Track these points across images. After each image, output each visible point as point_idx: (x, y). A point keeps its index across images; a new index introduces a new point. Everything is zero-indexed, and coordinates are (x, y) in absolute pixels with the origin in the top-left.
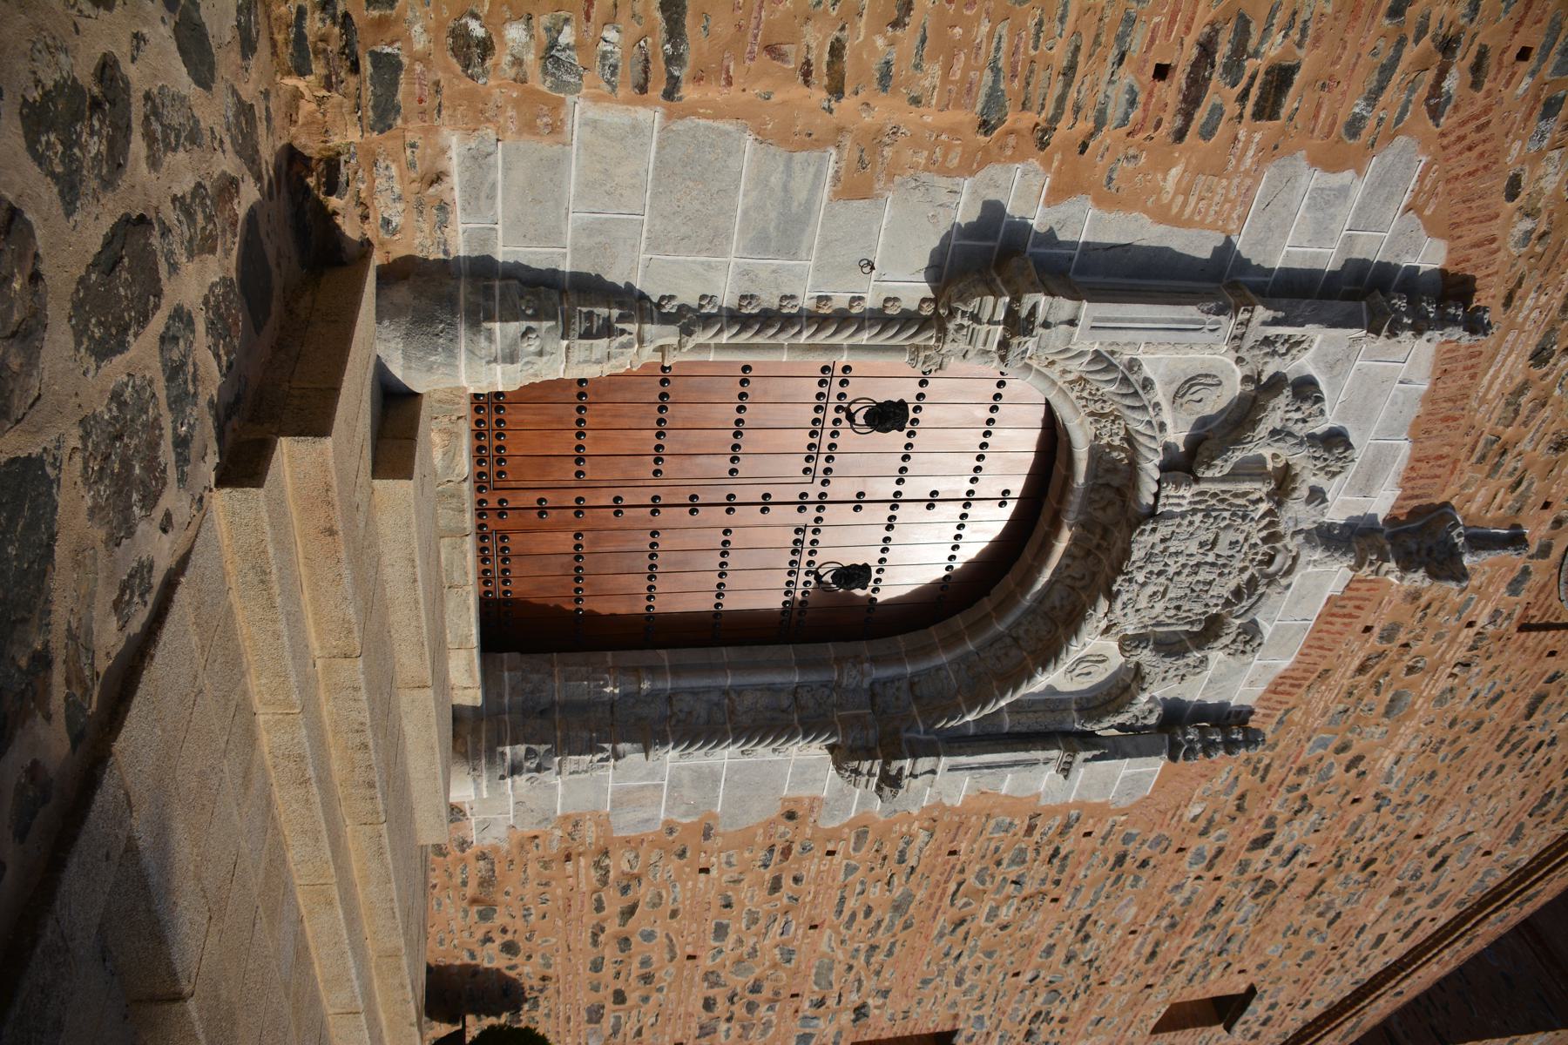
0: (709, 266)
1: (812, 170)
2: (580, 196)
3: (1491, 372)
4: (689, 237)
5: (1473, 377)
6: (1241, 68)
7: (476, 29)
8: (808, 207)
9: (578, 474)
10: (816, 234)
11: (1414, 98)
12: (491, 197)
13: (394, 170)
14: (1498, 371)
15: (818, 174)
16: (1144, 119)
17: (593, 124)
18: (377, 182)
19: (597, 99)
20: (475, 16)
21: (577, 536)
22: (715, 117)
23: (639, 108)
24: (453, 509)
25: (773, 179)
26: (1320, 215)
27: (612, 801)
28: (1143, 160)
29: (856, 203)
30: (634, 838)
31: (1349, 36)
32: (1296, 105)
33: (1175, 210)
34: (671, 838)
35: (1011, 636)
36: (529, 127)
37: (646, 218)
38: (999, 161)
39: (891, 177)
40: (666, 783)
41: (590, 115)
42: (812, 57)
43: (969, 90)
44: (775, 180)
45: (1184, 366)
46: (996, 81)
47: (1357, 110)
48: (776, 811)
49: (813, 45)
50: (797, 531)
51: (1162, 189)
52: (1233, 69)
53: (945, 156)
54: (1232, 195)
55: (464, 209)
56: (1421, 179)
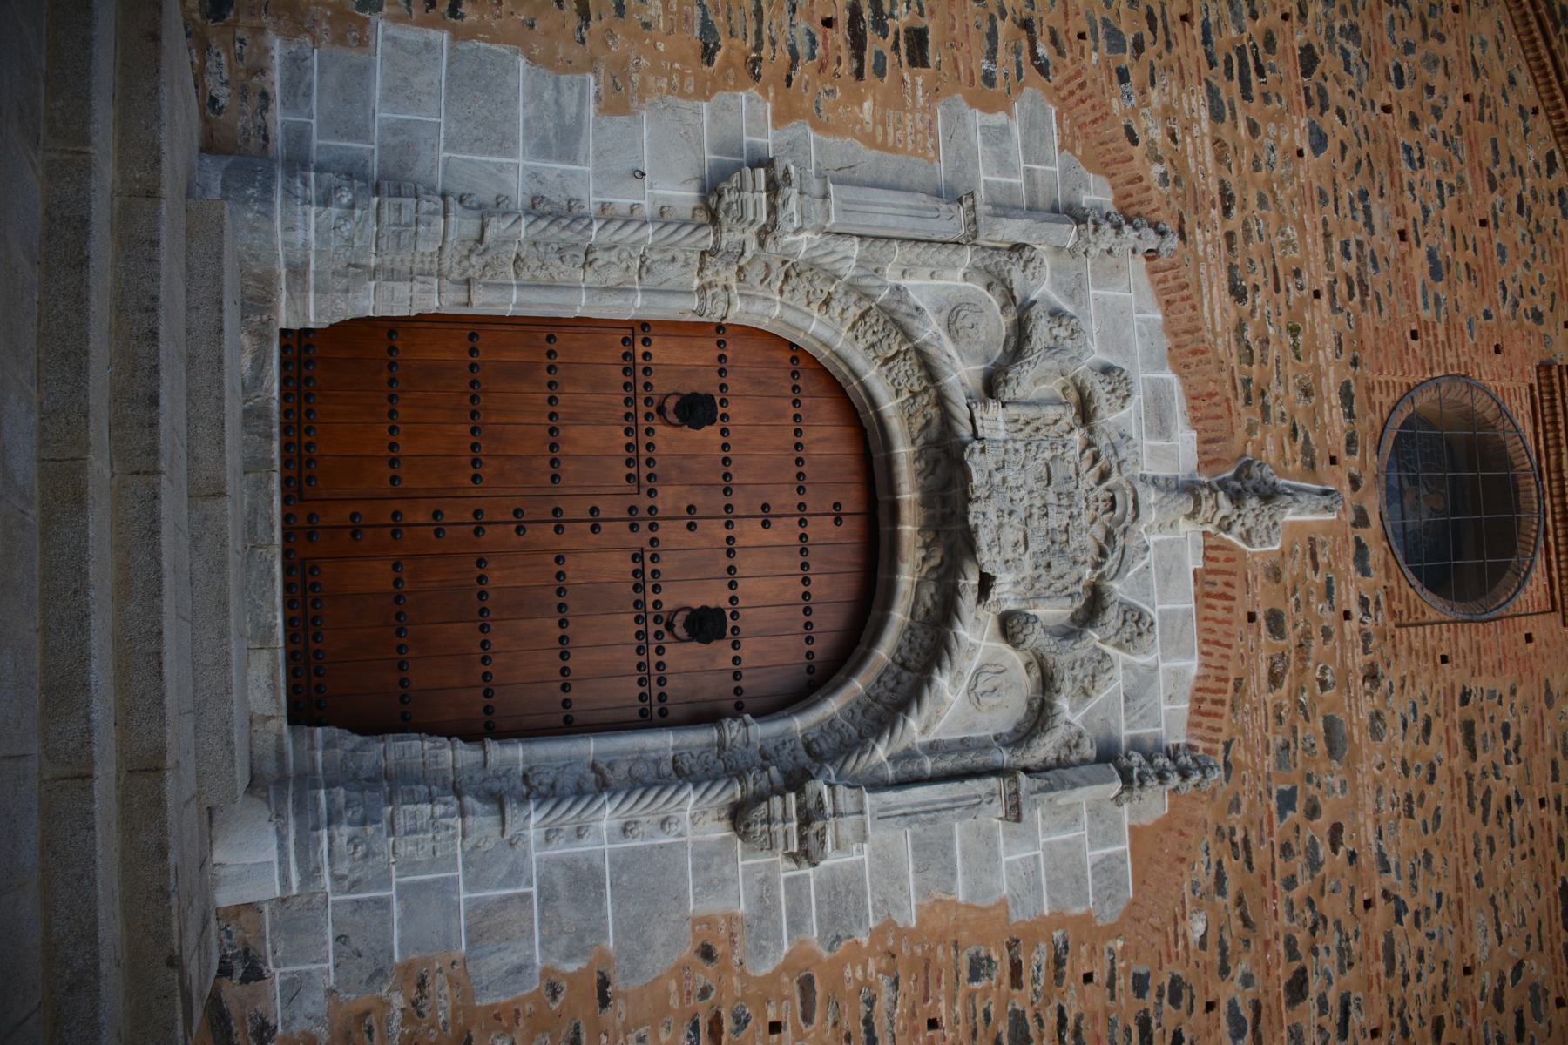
0: (501, 167)
1: (577, 89)
2: (384, 99)
3: (1206, 301)
4: (481, 140)
8: (579, 118)
9: (393, 479)
10: (589, 143)
11: (1021, 58)
12: (308, 95)
13: (224, 59)
14: (1211, 301)
15: (582, 94)
16: (827, 55)
17: (394, 40)
18: (209, 64)
19: (396, 19)
21: (395, 567)
22: (492, 41)
24: (260, 435)
25: (545, 95)
27: (468, 931)
28: (839, 94)
29: (618, 119)
30: (506, 1006)
31: (954, 11)
33: (880, 139)
34: (555, 1006)
36: (340, 40)
37: (442, 121)
38: (725, 90)
39: (642, 99)
40: (534, 890)
43: (687, 20)
44: (548, 95)
45: (944, 294)
46: (705, 14)
47: (985, 67)
48: (687, 951)
50: (634, 558)
53: (682, 82)
54: (920, 126)
55: (283, 103)
56: (1060, 125)
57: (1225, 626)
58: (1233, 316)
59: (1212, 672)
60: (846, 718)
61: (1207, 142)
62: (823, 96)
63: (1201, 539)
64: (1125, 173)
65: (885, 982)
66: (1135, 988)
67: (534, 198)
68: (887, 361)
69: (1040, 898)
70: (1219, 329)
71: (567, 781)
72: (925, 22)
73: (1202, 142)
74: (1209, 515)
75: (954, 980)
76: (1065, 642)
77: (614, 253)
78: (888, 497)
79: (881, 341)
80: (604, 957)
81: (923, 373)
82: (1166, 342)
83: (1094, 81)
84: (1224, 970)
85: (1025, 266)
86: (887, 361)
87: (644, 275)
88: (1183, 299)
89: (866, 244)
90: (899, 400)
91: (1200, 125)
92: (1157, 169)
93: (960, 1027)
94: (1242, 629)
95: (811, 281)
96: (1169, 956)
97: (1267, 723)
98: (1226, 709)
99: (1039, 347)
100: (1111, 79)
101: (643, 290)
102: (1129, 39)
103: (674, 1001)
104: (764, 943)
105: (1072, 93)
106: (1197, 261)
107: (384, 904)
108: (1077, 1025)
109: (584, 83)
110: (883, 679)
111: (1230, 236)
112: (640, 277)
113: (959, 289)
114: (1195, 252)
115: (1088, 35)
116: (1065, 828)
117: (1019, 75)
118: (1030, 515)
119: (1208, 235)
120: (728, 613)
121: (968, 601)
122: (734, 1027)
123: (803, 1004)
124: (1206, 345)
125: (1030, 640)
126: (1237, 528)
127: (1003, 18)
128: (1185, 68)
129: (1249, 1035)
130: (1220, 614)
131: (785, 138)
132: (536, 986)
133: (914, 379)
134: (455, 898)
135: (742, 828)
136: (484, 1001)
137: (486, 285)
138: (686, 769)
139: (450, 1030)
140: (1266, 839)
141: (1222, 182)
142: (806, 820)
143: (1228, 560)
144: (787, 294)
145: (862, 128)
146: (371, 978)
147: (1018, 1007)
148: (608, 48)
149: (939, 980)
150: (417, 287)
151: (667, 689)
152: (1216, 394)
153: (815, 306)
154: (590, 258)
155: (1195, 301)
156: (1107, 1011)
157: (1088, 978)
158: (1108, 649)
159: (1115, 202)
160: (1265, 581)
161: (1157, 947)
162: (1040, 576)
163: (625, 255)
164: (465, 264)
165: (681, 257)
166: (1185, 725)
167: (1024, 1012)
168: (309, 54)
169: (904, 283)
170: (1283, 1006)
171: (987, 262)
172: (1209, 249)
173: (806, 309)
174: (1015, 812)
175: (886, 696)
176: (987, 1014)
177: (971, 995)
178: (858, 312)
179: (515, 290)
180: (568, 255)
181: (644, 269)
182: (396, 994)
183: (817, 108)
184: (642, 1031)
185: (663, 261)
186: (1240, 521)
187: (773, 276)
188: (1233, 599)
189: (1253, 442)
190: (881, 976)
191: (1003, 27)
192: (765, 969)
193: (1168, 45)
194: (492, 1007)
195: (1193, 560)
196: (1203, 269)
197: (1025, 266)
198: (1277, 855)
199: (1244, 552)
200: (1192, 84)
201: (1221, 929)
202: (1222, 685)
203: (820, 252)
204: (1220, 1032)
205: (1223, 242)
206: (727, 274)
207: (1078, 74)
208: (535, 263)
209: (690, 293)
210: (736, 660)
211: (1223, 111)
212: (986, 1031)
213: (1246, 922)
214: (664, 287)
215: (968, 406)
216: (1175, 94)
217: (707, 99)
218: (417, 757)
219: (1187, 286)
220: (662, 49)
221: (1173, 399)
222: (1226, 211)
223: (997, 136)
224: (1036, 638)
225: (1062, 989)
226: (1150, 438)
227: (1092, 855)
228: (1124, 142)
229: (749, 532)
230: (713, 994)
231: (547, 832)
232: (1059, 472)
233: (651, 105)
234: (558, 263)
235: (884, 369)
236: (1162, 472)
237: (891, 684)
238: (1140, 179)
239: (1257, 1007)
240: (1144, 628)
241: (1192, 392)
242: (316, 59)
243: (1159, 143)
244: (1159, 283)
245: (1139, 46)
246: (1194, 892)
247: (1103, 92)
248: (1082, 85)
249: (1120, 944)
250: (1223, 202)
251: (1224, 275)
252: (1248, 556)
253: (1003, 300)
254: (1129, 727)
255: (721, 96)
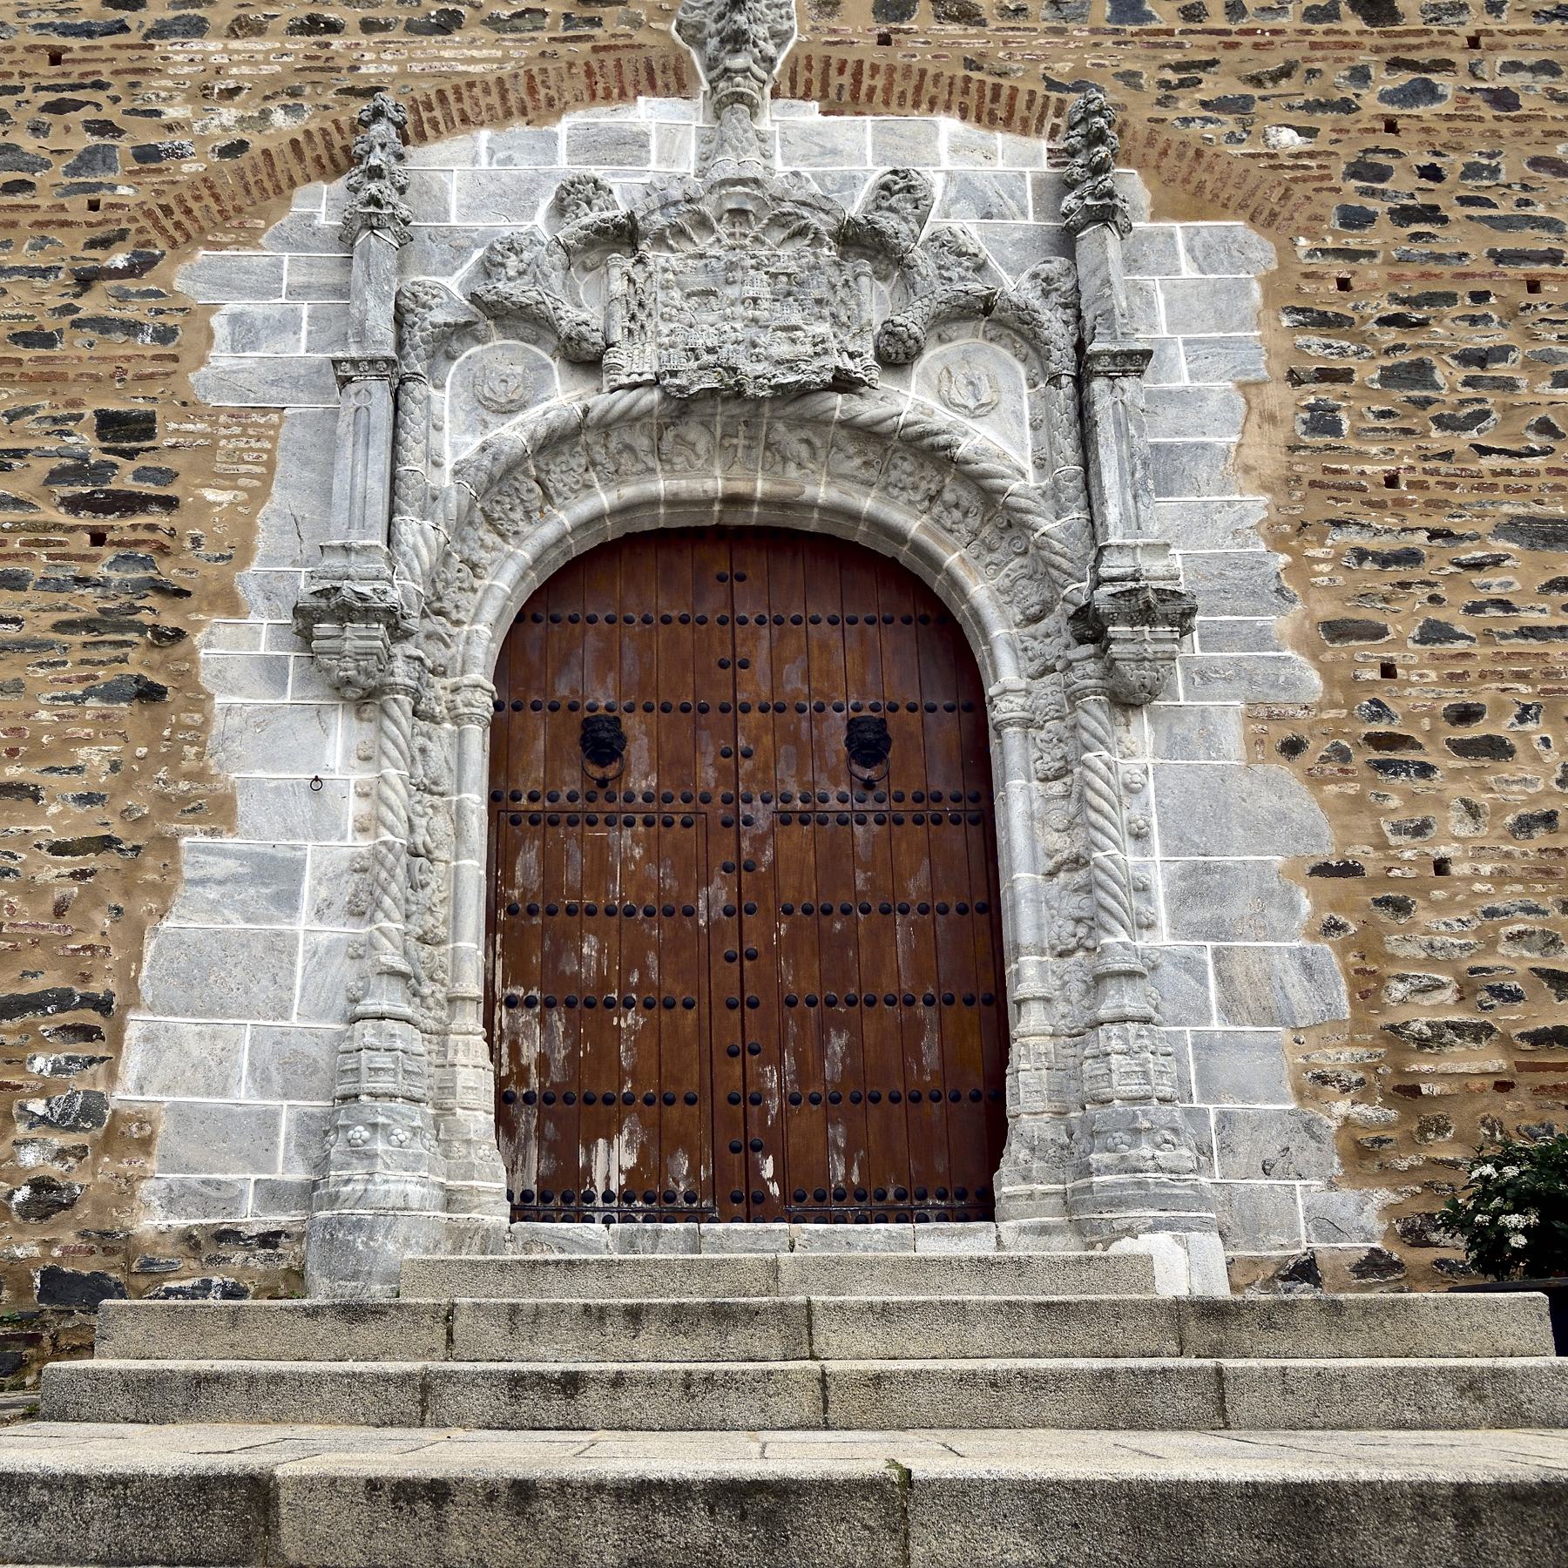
1: (202, 858)
3: (461, 68)
5: (471, 85)
6: (98, 466)
7: (23, 1193)
11: (133, 290)
12: (219, 1185)
15: (208, 851)
19: (112, 1076)
20: (10, 1195)
23: (127, 1035)
25: (211, 896)
26: (263, 333)
28: (198, 532)
29: (241, 807)
30: (1353, 985)
32: (141, 400)
33: (256, 483)
34: (1353, 928)
35: (930, 509)
36: (145, 1144)
38: (197, 675)
41: (130, 1085)
42: (66, 871)
44: (212, 893)
45: (461, 415)
48: (1285, 771)
49: (56, 872)
51: (231, 503)
52: (102, 471)
54: (237, 430)
57: (897, 76)
58: (481, 32)
59: (957, 98)
60: (996, 572)
61: (235, 44)
62: (202, 551)
63: (781, 102)
64: (286, 163)
65: (1337, 537)
66: (1361, 226)
67: (352, 914)
68: (547, 497)
69: (1239, 340)
70: (499, 54)
71: (1075, 904)
72: (88, 413)
73: (238, 52)
74: (755, 84)
75: (1337, 452)
76: (918, 287)
77: (417, 821)
78: (717, 508)
79: (522, 501)
80: (1286, 873)
81: (565, 449)
82: (518, 127)
83: (159, 193)
84: (1346, 106)
85: (424, 306)
86: (547, 497)
87: (440, 789)
88: (459, 99)
89: (404, 506)
90: (597, 485)
91: (212, 53)
92: (279, 118)
93: (1398, 449)
94: (899, 55)
95: (447, 583)
96: (1322, 178)
97: (1025, 29)
98: (1006, 83)
99: (534, 294)
100: (154, 171)
101: (459, 791)
102: (94, 140)
103: (1352, 789)
104: (1282, 679)
105: (178, 225)
106: (404, 74)
107: (1225, 1118)
108: (1403, 302)
109: (193, 849)
110: (948, 525)
111: (368, 26)
112: (442, 795)
113: (455, 396)
114: (394, 77)
115: (93, 196)
116: (1150, 304)
117: (158, 294)
118: (755, 320)
119: (368, 56)
120: (853, 714)
121: (866, 409)
122: (1386, 720)
123: (1360, 638)
124: (521, 72)
125: (915, 329)
126: (770, 49)
127: (77, 310)
128: (131, 66)
129: (1434, 78)
130: (880, 82)
131: (261, 603)
132: (1327, 947)
133: (574, 463)
134: (1218, 1036)
135: (1144, 695)
136: (1346, 1011)
137: (455, 979)
138: (1057, 765)
139: (1380, 1050)
140: (1178, 38)
141: (292, 30)
142: (1146, 615)
143: (809, 67)
144: (462, 616)
145: (243, 504)
146: (1313, 1136)
147: (1376, 376)
148: (144, 818)
149: (1336, 471)
150: (461, 1058)
151: (947, 792)
152: (587, 64)
153: (477, 583)
154: (423, 851)
155: (462, 82)
156: (1388, 262)
157: (1344, 284)
158: (925, 234)
159: (328, 180)
160: (836, 19)
161: (1311, 193)
162: (832, 315)
163: (419, 808)
164: (431, 1001)
165: (420, 741)
166: (1024, 139)
167: (1383, 368)
168: (163, 1184)
169: (449, 465)
170: (1397, 28)
171: (421, 352)
172: (389, 57)
173: (480, 594)
174: (1136, 361)
175: (973, 522)
176: (1383, 415)
177: (1357, 434)
178: (486, 526)
179: (459, 944)
180: (419, 877)
181: (434, 788)
182: (1334, 1110)
183: (217, 559)
184: (1386, 828)
185: (425, 764)
186: (761, 43)
187: (441, 630)
188: (860, 63)
189: (650, 19)
190: (1329, 542)
191: (89, 306)
192: (1315, 679)
193: (100, 86)
194: (1351, 997)
195: (808, 114)
196: (416, 68)
197: (424, 306)
198: (1198, 26)
199: (799, 43)
200: (153, 58)
201: (1290, 108)
202: (973, 87)
203: (416, 564)
204: (1426, 116)
205: (378, 37)
206: (438, 686)
207: (149, 214)
208: (430, 920)
209: (461, 734)
210: (912, 708)
211: (190, 18)
212: (1403, 417)
213: (1286, 72)
214: (453, 765)
215: (613, 391)
216: (170, 84)
217: (211, 697)
218: (1040, 1078)
219: (441, 93)
220: (145, 750)
221: (595, 124)
222: (334, 28)
223: (246, 333)
224: (912, 320)
225: (1357, 319)
226: (648, 161)
227: (1188, 270)
228: (244, 160)
229: (756, 685)
230: (1344, 743)
231: (1140, 926)
232: (700, 282)
233: (221, 767)
234: (428, 890)
235: (558, 501)
236: (692, 149)
237: (957, 514)
238: (294, 143)
239: (1395, 65)
240: (902, 184)
241: (586, 97)
242: (171, 1176)
243: (240, 113)
244: (438, 131)
245: (103, 127)
246: (1241, 141)
247: (173, 183)
248: (167, 210)
249: (1302, 241)
250: (320, 32)
251: (426, 41)
252: (804, 39)
253: (469, 340)
254: (1024, 214)
255: (205, 677)
